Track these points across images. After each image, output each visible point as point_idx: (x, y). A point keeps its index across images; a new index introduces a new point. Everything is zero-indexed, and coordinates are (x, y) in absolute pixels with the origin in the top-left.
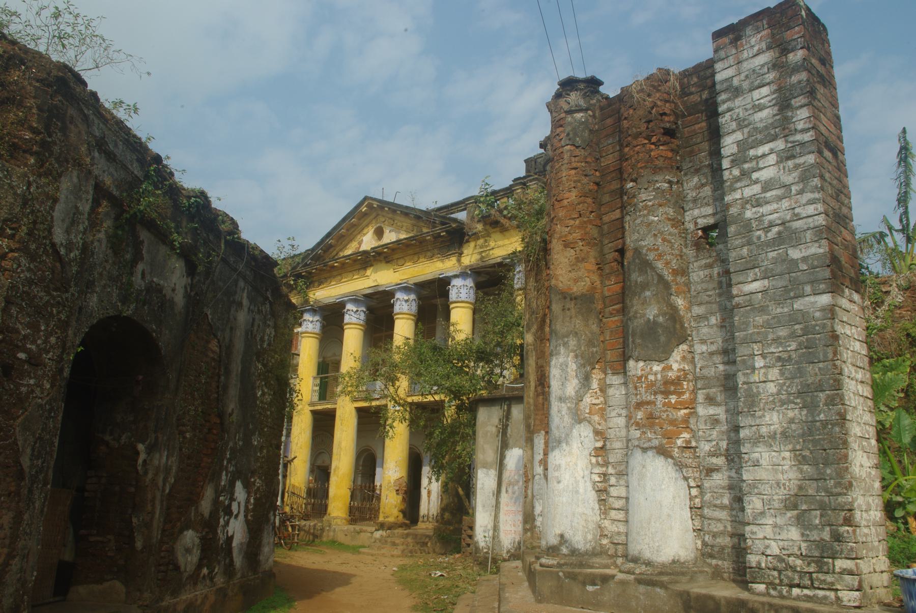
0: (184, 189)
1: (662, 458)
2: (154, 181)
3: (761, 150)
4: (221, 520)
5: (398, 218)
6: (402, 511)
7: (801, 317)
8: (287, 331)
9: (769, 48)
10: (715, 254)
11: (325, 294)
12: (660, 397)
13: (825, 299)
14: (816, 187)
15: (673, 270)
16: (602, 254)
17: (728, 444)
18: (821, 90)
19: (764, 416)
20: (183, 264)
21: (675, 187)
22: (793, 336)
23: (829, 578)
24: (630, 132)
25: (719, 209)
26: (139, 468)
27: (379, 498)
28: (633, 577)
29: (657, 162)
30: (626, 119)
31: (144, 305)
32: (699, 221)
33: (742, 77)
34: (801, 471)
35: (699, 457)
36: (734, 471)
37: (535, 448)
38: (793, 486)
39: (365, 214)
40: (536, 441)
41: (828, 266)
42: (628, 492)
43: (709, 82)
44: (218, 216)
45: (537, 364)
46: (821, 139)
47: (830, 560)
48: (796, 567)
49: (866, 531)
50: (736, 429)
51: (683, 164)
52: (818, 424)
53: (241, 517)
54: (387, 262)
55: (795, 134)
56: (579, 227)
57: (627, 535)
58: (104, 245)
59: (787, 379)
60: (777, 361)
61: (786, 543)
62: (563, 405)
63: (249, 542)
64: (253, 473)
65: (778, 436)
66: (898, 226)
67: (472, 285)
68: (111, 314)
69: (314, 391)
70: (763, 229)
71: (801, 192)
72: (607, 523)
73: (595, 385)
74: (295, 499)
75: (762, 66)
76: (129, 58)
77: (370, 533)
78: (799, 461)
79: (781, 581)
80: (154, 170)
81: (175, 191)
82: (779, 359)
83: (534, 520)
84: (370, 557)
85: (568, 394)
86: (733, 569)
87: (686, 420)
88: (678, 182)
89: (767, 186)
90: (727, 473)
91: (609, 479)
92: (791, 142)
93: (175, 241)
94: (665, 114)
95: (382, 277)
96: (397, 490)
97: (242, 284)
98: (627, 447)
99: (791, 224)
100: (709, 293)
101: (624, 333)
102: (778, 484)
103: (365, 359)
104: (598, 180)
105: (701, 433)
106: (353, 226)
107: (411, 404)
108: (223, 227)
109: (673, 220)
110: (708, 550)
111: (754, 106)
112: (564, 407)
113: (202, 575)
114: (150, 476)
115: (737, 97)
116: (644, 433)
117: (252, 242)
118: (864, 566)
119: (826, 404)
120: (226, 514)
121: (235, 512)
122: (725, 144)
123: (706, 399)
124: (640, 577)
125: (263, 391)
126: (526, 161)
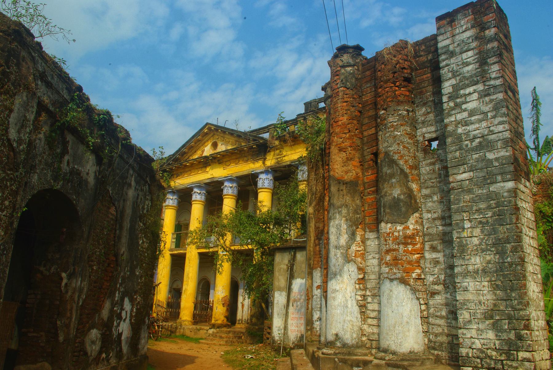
0: (96, 109)
1: (403, 286)
2: (77, 103)
3: (467, 91)
4: (115, 323)
5: (227, 136)
6: (226, 317)
7: (496, 196)
8: (159, 203)
9: (472, 27)
10: (436, 156)
11: (181, 182)
12: (401, 247)
13: (510, 185)
14: (504, 114)
15: (410, 166)
16: (363, 156)
17: (445, 277)
18: (505, 54)
19: (471, 259)
20: (94, 157)
21: (411, 114)
22: (489, 208)
23: (514, 364)
24: (382, 79)
25: (439, 128)
26: (63, 289)
27: (212, 309)
28: (384, 362)
29: (400, 98)
30: (379, 71)
31: (68, 182)
32: (426, 135)
33: (456, 45)
34: (495, 295)
35: (426, 285)
36: (449, 294)
37: (314, 279)
38: (490, 303)
39: (206, 134)
40: (314, 274)
41: (512, 164)
42: (380, 307)
43: (433, 49)
44: (118, 127)
45: (315, 226)
46: (506, 84)
47: (515, 352)
48: (492, 356)
49: (537, 333)
50: (452, 267)
51: (416, 100)
52: (506, 264)
53: (128, 320)
54: (220, 163)
55: (490, 81)
56: (348, 139)
57: (379, 334)
58: (43, 143)
59: (485, 235)
60: (479, 224)
61: (485, 341)
62: (338, 251)
63: (132, 337)
64: (136, 292)
65: (480, 272)
66: (532, 146)
67: (272, 178)
68: (47, 188)
69: (172, 242)
70: (469, 140)
71: (494, 117)
72: (365, 327)
73: (358, 239)
74: (160, 308)
75: (469, 38)
76: (62, 30)
77: (207, 331)
78: (494, 288)
79: (482, 365)
80: (77, 96)
81: (90, 110)
82: (480, 222)
83: (313, 323)
84: (206, 345)
85: (341, 244)
86: (449, 357)
87: (418, 261)
88: (413, 110)
89: (472, 113)
90: (444, 296)
91: (367, 299)
92: (487, 86)
93: (90, 141)
94: (404, 68)
95: (217, 172)
96: (223, 304)
97: (131, 172)
98: (379, 278)
99: (488, 137)
100: (432, 181)
101: (378, 207)
102: (480, 303)
103: (205, 222)
104: (360, 109)
105: (427, 270)
106: (199, 140)
107: (235, 250)
108: (121, 135)
109: (410, 134)
110: (432, 344)
111: (463, 63)
112: (339, 253)
113: (102, 358)
114: (70, 293)
115: (452, 57)
116: (392, 269)
117: (138, 145)
118: (537, 356)
119: (511, 252)
120: (118, 319)
121: (124, 318)
122: (445, 86)
123: (431, 248)
124: (389, 362)
125: (143, 240)
126: (305, 104)
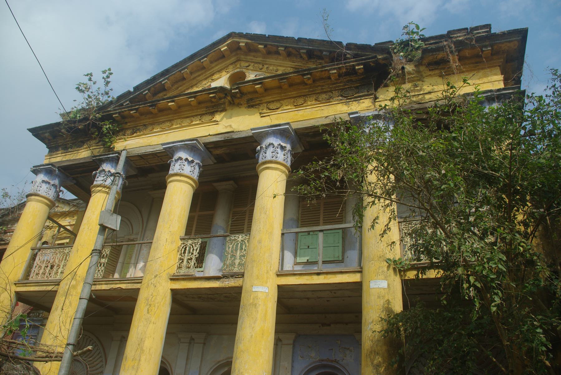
39: (222, 56)
95: (240, 123)
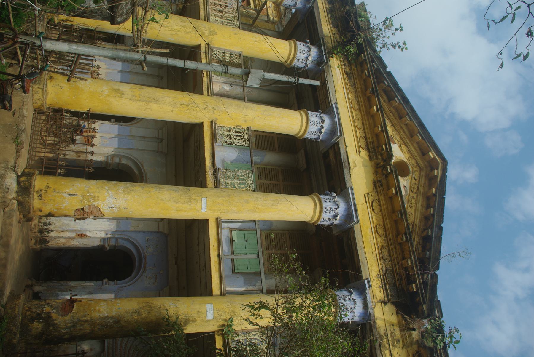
39: (424, 153)
95: (359, 175)
